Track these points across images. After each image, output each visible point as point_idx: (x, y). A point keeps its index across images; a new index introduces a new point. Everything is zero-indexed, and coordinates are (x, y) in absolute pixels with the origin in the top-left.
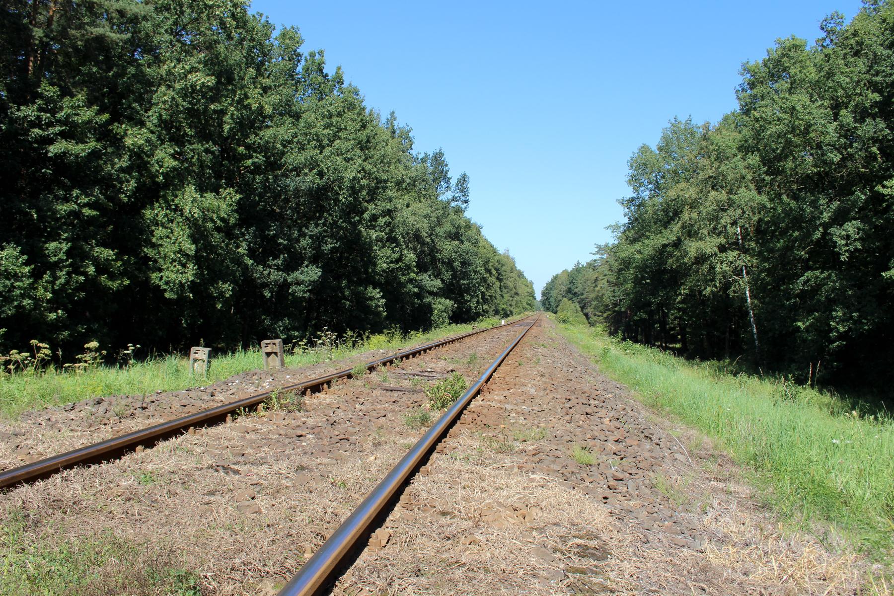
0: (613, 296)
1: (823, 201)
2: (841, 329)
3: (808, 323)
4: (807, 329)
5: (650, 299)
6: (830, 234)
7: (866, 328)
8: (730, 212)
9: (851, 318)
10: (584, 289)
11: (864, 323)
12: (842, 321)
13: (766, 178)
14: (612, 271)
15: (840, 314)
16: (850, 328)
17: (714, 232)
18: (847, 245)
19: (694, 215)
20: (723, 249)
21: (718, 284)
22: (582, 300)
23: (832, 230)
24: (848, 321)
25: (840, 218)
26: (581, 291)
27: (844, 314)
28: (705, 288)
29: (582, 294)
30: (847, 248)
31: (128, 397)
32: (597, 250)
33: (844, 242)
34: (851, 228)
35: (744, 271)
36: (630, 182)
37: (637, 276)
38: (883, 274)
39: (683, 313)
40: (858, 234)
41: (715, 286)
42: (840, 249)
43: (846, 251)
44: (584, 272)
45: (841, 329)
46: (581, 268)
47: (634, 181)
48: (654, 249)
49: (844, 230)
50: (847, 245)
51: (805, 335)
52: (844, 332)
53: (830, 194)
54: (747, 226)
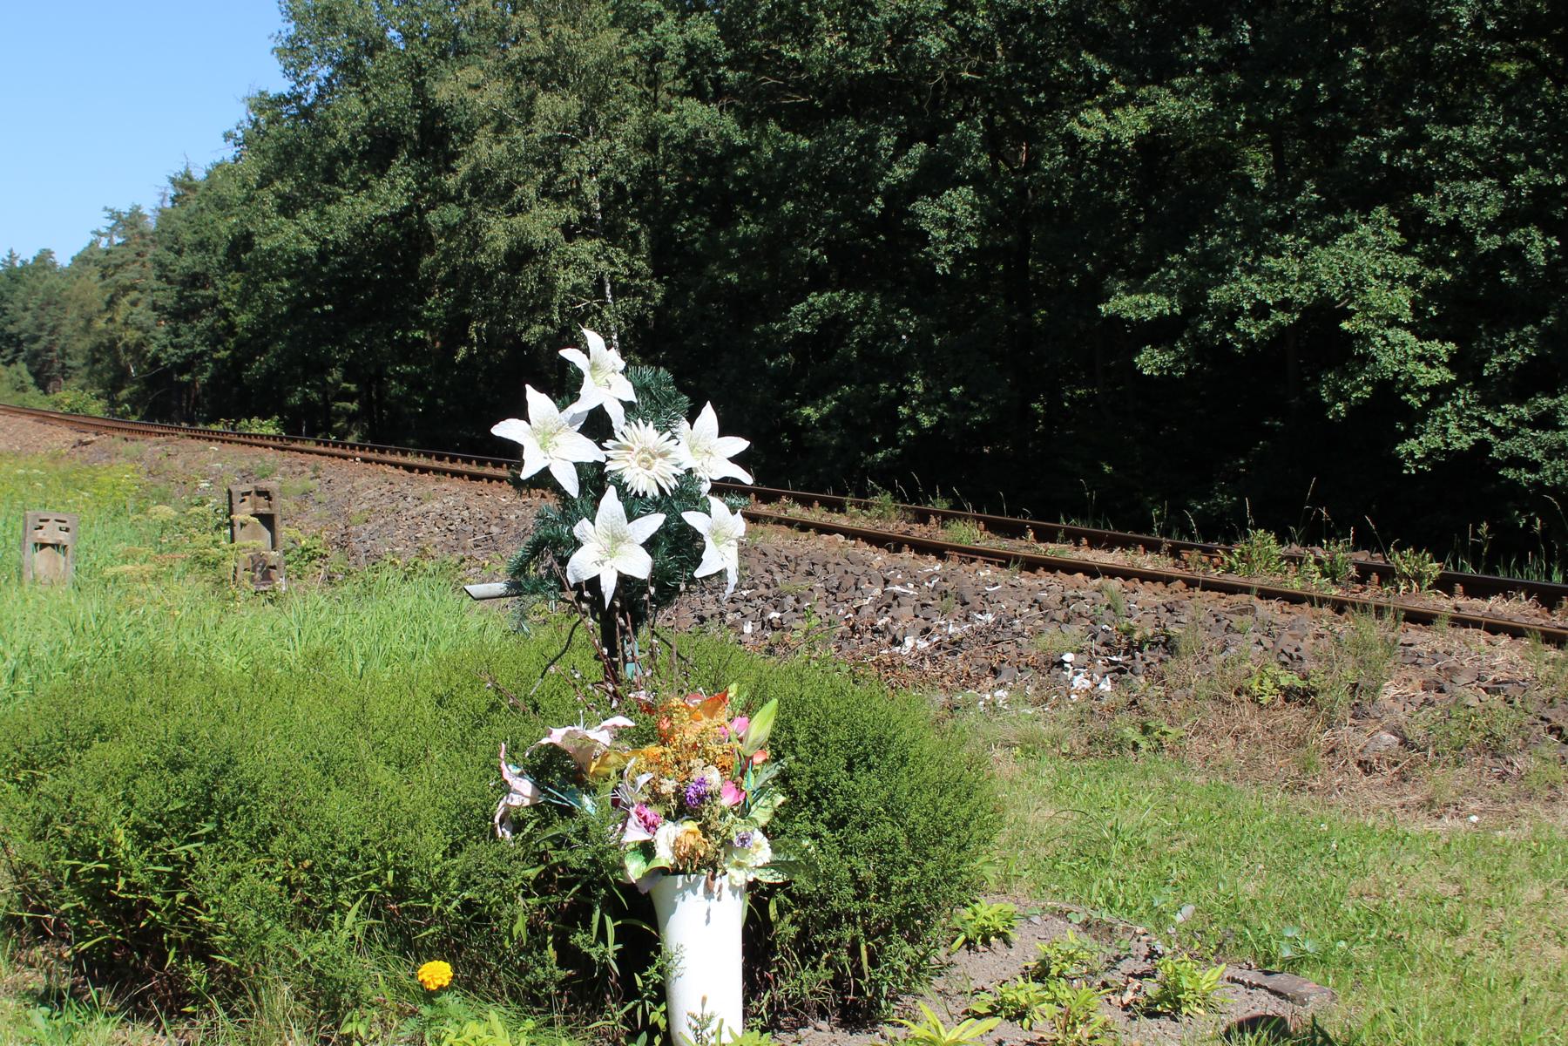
0: (174, 346)
1: (886, 141)
2: (926, 421)
3: (826, 410)
4: (824, 421)
5: (328, 351)
6: (912, 214)
7: (979, 418)
8: (588, 146)
9: (947, 396)
10: (41, 327)
11: (972, 409)
12: (927, 403)
13: (730, 75)
14: (170, 281)
15: (919, 388)
16: (941, 418)
17: (547, 191)
18: (949, 240)
19: (499, 150)
20: (569, 232)
21: (556, 317)
22: (36, 355)
23: (920, 206)
24: (937, 403)
25: (935, 178)
26: (32, 330)
27: (927, 389)
28: (527, 328)
29: (35, 339)
30: (950, 247)
31: (1105, 985)
32: (110, 223)
33: (943, 233)
34: (960, 200)
35: (608, 288)
36: (280, 53)
37: (301, 294)
38: (1102, 308)
39: (411, 387)
40: (973, 215)
41: (552, 323)
42: (937, 250)
43: (948, 253)
44: (33, 282)
45: (926, 421)
46: (21, 270)
47: (293, 54)
48: (351, 230)
49: (942, 207)
50: (949, 240)
51: (821, 436)
52: (932, 428)
53: (901, 124)
54: (622, 179)
